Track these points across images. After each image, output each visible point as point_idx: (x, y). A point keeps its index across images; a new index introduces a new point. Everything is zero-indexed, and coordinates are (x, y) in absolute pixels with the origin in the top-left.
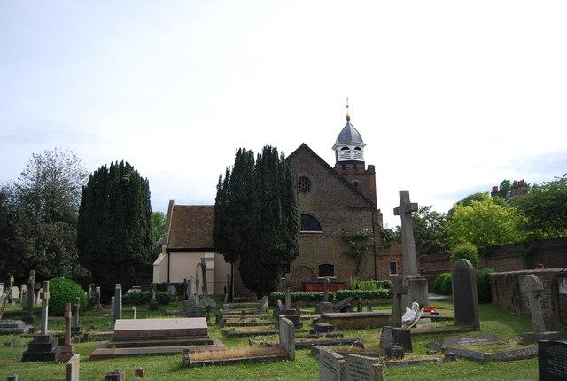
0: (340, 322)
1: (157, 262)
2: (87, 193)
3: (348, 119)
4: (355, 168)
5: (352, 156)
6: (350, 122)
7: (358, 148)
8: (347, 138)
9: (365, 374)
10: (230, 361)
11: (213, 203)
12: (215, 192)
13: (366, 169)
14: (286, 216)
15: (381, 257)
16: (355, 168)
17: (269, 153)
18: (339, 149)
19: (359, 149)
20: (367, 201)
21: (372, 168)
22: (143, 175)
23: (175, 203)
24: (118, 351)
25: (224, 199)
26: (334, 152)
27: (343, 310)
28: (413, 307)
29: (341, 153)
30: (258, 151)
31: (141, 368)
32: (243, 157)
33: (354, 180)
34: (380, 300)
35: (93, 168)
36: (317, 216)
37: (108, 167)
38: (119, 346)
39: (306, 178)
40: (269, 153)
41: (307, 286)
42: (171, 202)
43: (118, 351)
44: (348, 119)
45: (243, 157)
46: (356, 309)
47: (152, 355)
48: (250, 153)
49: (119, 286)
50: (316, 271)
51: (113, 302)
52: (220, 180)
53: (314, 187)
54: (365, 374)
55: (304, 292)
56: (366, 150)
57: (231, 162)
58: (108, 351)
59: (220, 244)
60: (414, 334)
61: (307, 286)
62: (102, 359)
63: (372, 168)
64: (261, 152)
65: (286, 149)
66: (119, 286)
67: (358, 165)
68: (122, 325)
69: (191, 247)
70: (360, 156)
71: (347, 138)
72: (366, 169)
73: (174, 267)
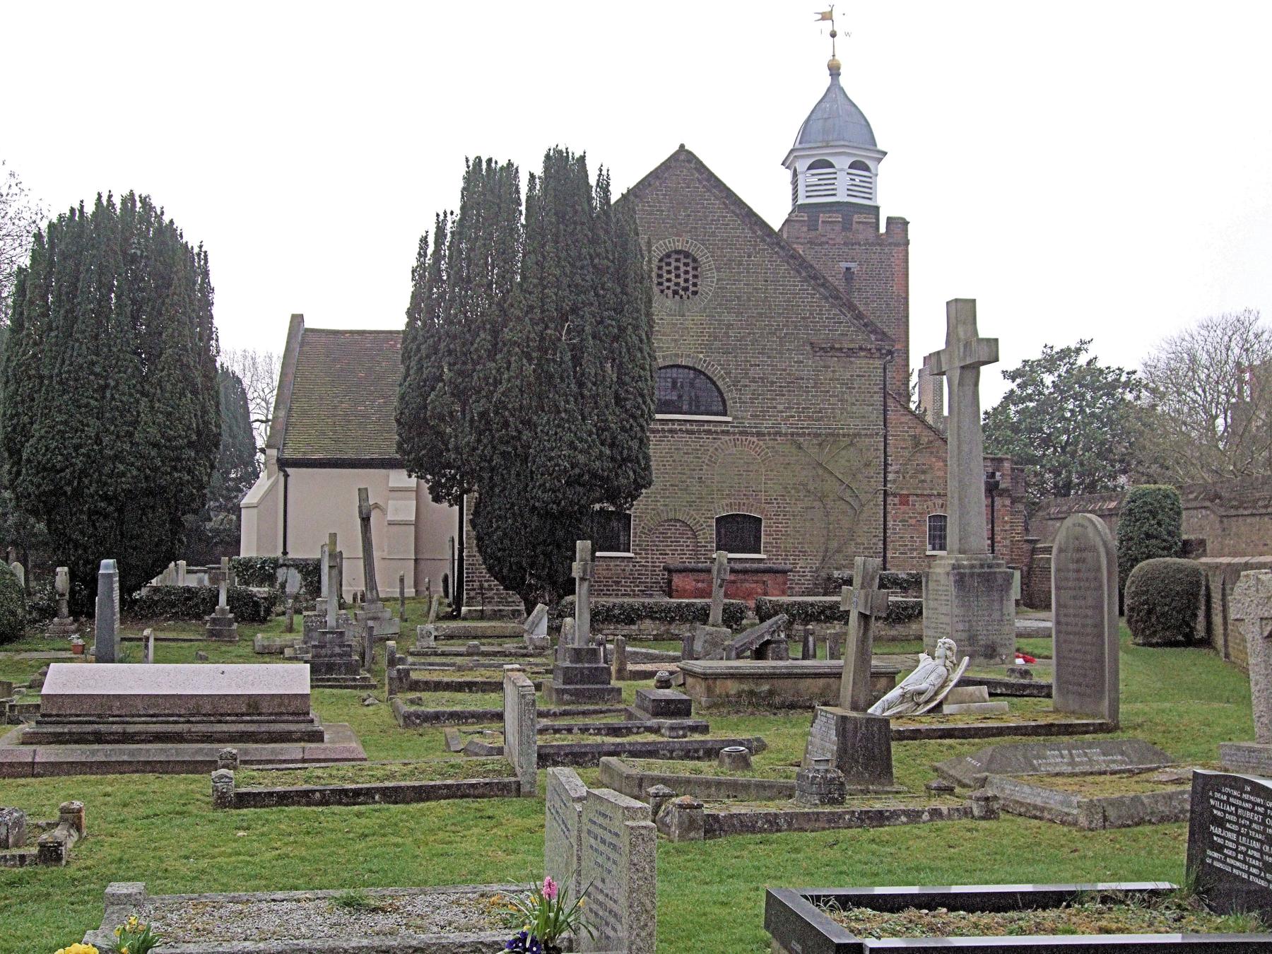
0: (733, 687)
1: (251, 496)
3: (834, 70)
6: (843, 81)
8: (836, 134)
10: (345, 792)
11: (398, 322)
12: (404, 291)
13: (883, 229)
14: (597, 379)
15: (904, 500)
16: (847, 226)
17: (564, 170)
18: (802, 165)
19: (867, 169)
20: (871, 328)
21: (899, 225)
22: (191, 238)
23: (309, 324)
24: (46, 754)
25: (431, 313)
26: (789, 173)
27: (760, 654)
28: (939, 652)
29: (806, 179)
30: (503, 162)
31: (77, 804)
32: (487, 184)
33: (841, 260)
34: (226, 708)
35: (56, 206)
36: (715, 371)
37: (90, 209)
38: (58, 739)
39: (687, 255)
40: (564, 170)
41: (677, 580)
42: (297, 320)
43: (46, 754)
44: (834, 70)
45: (487, 184)
46: (797, 650)
48: (510, 170)
50: (709, 534)
52: (422, 254)
53: (708, 285)
55: (671, 597)
56: (886, 175)
57: (449, 198)
59: (423, 449)
60: (901, 736)
61: (677, 580)
63: (899, 225)
64: (539, 171)
65: (622, 165)
67: (856, 218)
68: (70, 678)
69: (351, 455)
70: (869, 189)
71: (836, 134)
72: (883, 229)
73: (281, 515)
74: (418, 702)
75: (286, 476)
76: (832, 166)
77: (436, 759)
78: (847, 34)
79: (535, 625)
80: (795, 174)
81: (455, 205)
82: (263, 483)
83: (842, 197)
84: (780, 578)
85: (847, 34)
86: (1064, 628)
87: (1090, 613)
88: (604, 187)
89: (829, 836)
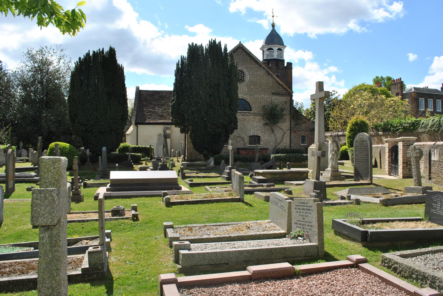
2: (73, 75)
3: (273, 26)
4: (277, 65)
5: (275, 55)
7: (279, 49)
9: (310, 210)
13: (285, 65)
15: (295, 132)
18: (265, 49)
21: (290, 64)
23: (140, 89)
26: (261, 52)
30: (205, 44)
31: (136, 205)
36: (248, 100)
37: (91, 54)
42: (138, 88)
47: (142, 196)
49: (104, 149)
50: (247, 140)
51: (100, 160)
54: (310, 210)
58: (227, 182)
59: (180, 120)
62: (126, 198)
66: (104, 149)
70: (282, 55)
72: (285, 65)
74: (192, 181)
75: (137, 127)
76: (273, 49)
77: (204, 194)
78: (277, 17)
79: (211, 162)
80: (263, 52)
81: (186, 55)
82: (131, 128)
83: (275, 57)
84: (265, 151)
85: (277, 17)
86: (357, 160)
87: (365, 156)
88: (226, 49)
89: (83, 223)
